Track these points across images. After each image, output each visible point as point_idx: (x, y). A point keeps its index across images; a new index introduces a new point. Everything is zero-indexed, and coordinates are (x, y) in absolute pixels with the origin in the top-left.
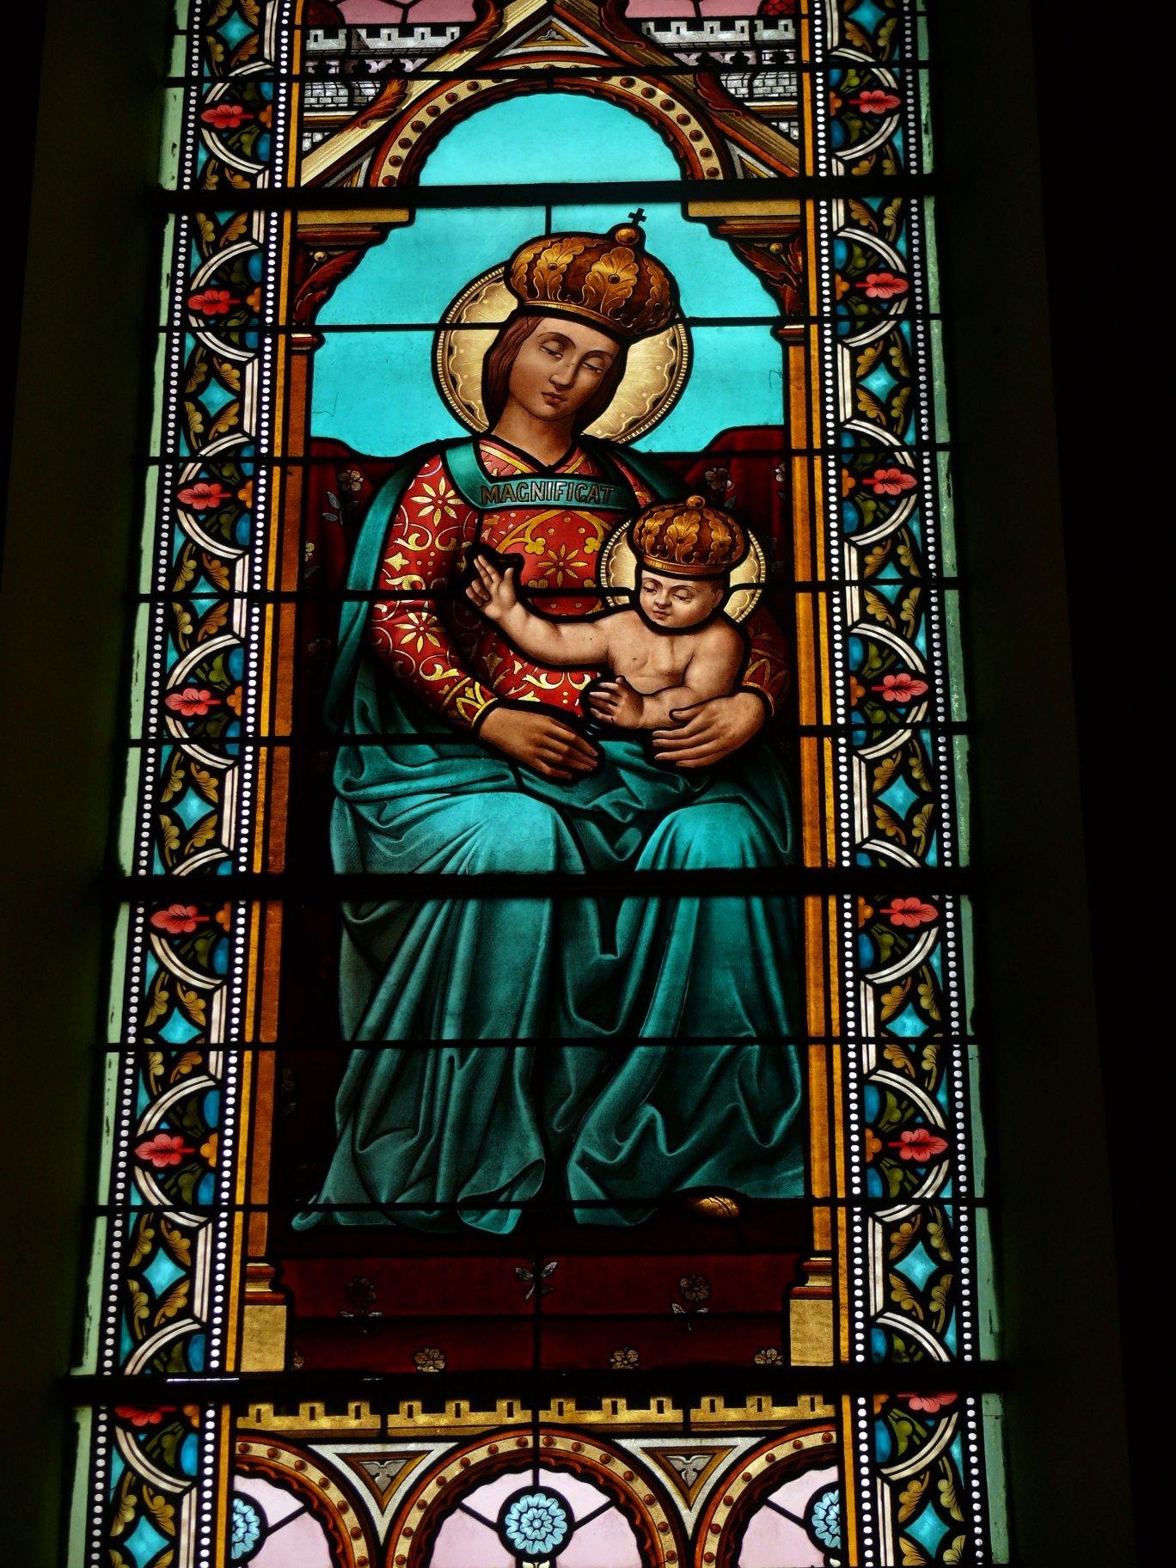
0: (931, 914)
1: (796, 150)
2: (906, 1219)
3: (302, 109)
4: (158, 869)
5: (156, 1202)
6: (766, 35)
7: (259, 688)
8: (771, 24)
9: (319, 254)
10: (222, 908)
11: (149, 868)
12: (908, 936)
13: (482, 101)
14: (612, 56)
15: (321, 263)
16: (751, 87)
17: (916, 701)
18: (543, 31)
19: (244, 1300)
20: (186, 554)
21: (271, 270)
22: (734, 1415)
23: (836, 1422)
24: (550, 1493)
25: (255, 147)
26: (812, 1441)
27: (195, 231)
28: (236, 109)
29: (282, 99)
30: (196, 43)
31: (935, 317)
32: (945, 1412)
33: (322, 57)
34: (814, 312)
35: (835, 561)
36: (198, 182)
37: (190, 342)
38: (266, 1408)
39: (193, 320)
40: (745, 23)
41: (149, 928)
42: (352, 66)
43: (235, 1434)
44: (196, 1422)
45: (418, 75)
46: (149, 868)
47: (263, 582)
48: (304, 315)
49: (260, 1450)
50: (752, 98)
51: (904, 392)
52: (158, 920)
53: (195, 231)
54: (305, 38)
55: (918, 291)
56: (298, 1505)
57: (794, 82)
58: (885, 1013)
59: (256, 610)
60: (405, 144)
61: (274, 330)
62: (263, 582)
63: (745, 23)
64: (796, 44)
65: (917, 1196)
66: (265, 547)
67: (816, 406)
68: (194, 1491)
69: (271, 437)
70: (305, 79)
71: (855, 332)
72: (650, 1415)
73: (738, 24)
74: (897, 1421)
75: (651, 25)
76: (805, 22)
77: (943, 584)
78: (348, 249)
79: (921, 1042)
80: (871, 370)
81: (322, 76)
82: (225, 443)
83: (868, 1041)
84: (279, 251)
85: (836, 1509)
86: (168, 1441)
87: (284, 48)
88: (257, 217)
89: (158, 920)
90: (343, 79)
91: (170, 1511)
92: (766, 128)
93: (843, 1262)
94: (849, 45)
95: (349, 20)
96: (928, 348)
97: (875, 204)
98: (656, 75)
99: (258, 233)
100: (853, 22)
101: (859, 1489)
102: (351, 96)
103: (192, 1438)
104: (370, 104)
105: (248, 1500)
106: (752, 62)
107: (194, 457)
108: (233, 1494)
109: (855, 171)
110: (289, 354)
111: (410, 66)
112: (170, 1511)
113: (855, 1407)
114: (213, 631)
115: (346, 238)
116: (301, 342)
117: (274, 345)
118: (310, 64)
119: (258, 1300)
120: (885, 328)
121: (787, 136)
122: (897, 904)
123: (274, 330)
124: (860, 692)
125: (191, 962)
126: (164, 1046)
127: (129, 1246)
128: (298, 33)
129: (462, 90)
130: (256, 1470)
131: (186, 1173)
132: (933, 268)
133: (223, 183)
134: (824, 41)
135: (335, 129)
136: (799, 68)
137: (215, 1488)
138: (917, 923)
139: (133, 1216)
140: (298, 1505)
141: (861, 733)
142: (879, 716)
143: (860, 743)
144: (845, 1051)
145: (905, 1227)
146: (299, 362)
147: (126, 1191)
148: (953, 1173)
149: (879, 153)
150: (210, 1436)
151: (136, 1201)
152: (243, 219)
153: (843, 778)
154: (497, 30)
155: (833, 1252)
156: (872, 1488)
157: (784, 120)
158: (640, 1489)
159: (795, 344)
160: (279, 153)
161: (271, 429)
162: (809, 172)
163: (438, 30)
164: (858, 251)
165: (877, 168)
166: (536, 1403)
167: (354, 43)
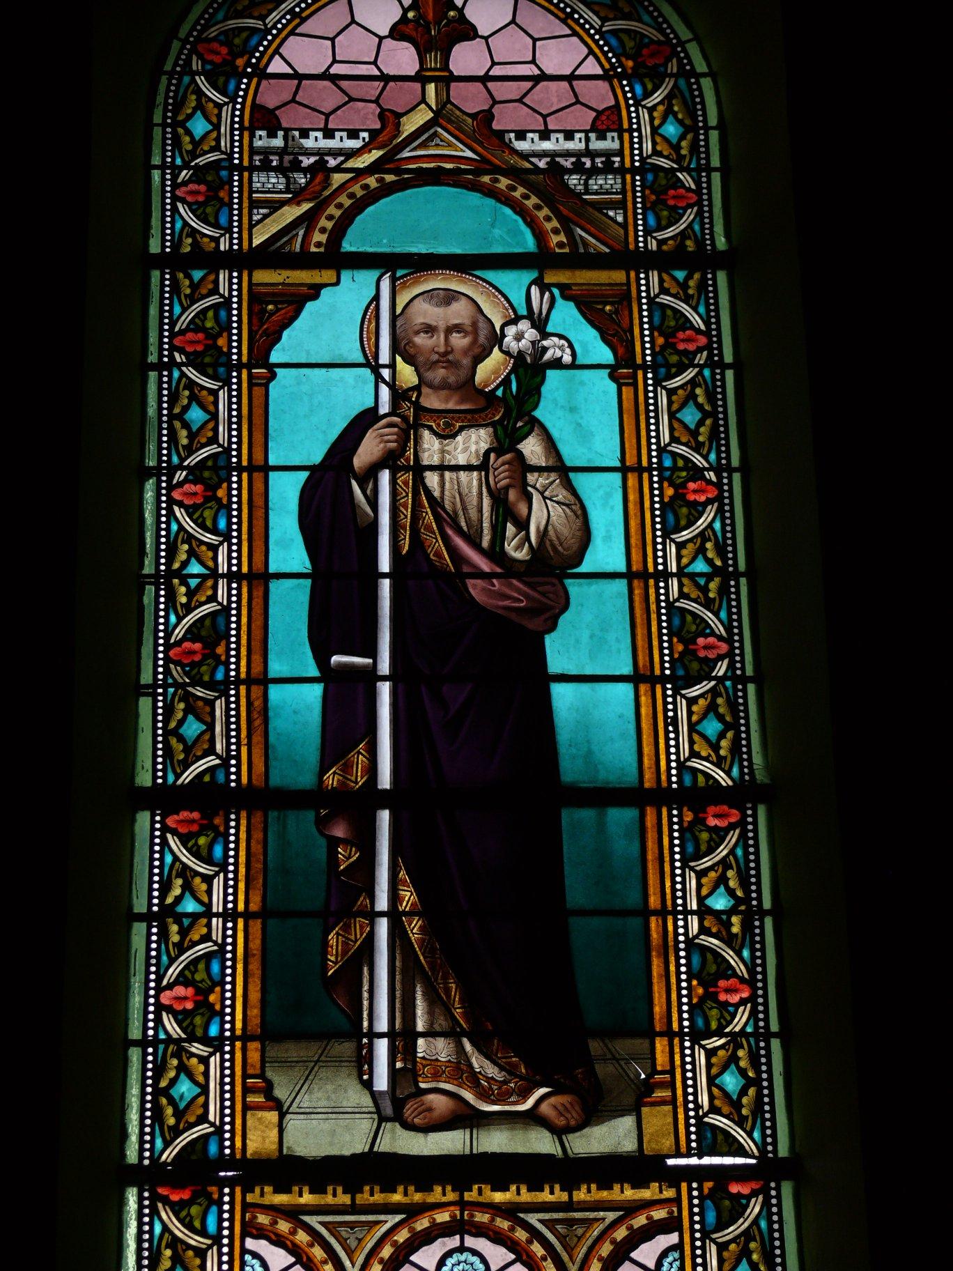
0: (735, 816)
1: (622, 231)
2: (722, 1047)
3: (251, 192)
4: (171, 778)
5: (175, 1036)
6: (596, 145)
7: (237, 842)
8: (602, 137)
9: (270, 307)
10: (218, 814)
11: (164, 777)
12: (719, 835)
13: (386, 190)
14: (484, 160)
15: (272, 314)
16: (586, 184)
17: (700, 350)
18: (431, 138)
19: (246, 1107)
20: (174, 873)
21: (236, 212)
22: (605, 1194)
23: (677, 1201)
24: (475, 1252)
25: (217, 218)
26: (659, 1214)
27: (176, 288)
28: (198, 646)
29: (233, 632)
30: (162, 593)
31: (716, 169)
32: (754, 1194)
33: (267, 152)
34: (639, 361)
35: (653, 427)
36: (176, 245)
37: (176, 374)
38: (268, 1189)
39: (177, 355)
40: (582, 135)
41: (165, 829)
42: (288, 162)
43: (246, 1206)
44: (216, 1196)
45: (338, 169)
46: (164, 777)
47: (239, 565)
48: (260, 356)
49: (263, 1219)
50: (587, 192)
51: (708, 422)
52: (170, 822)
53: (176, 288)
54: (252, 136)
55: (737, 651)
56: (293, 1260)
57: (619, 181)
58: (694, 718)
59: (230, 925)
60: (330, 218)
61: (240, 366)
62: (239, 565)
63: (582, 135)
64: (620, 153)
65: (727, 1030)
66: (239, 537)
67: (655, 643)
68: (222, 875)
69: (239, 450)
70: (252, 169)
71: (670, 377)
72: (545, 1196)
73: (578, 136)
74: (710, 1009)
75: (512, 135)
76: (626, 136)
77: (737, 575)
78: (290, 303)
79: (709, 577)
80: (704, 716)
81: (266, 167)
82: (204, 453)
83: (692, 913)
84: (240, 303)
85: (678, 1263)
86: (207, 513)
87: (237, 144)
88: (223, 276)
89: (170, 822)
90: (280, 170)
91: (202, 1068)
92: (597, 214)
93: (629, 198)
94: (660, 154)
95: (284, 125)
96: (734, 545)
97: (680, 275)
98: (515, 173)
99: (223, 288)
100: (718, 1087)
101: (694, 1248)
102: (288, 184)
103: (217, 1020)
104: (303, 189)
105: (255, 1255)
106: (588, 165)
107: (186, 166)
108: (244, 1251)
109: (665, 248)
110: (251, 385)
111: (332, 162)
112: (202, 1068)
113: (690, 1189)
114: (203, 599)
115: (292, 295)
116: (259, 376)
117: (239, 377)
118: (257, 158)
119: (258, 1107)
120: (690, 374)
121: (613, 220)
122: (712, 809)
123: (240, 366)
124: (680, 648)
125: (204, 219)
126: (178, 918)
127: (159, 1071)
128: (246, 134)
129: (372, 181)
130: (260, 1234)
131: (200, 1010)
132: (754, 725)
133: (195, 244)
134: (640, 149)
135: (275, 206)
136: (622, 171)
137: (231, 1245)
138: (726, 823)
139: (161, 1047)
140: (293, 1260)
141: (663, 370)
142: (674, 359)
143: (711, 1228)
144: (675, 921)
145: (721, 1053)
146: (258, 391)
147: (155, 1029)
148: (754, 1013)
149: (683, 235)
150: (226, 1207)
151: (162, 1036)
152: (212, 277)
153: (660, 554)
154: (396, 137)
155: (672, 1072)
156: (674, 703)
157: (611, 209)
158: (537, 1249)
159: (627, 384)
160: (236, 218)
161: (239, 443)
162: (664, 784)
163: (353, 134)
164: (689, 618)
165: (682, 246)
166: (461, 1187)
167: (290, 142)
